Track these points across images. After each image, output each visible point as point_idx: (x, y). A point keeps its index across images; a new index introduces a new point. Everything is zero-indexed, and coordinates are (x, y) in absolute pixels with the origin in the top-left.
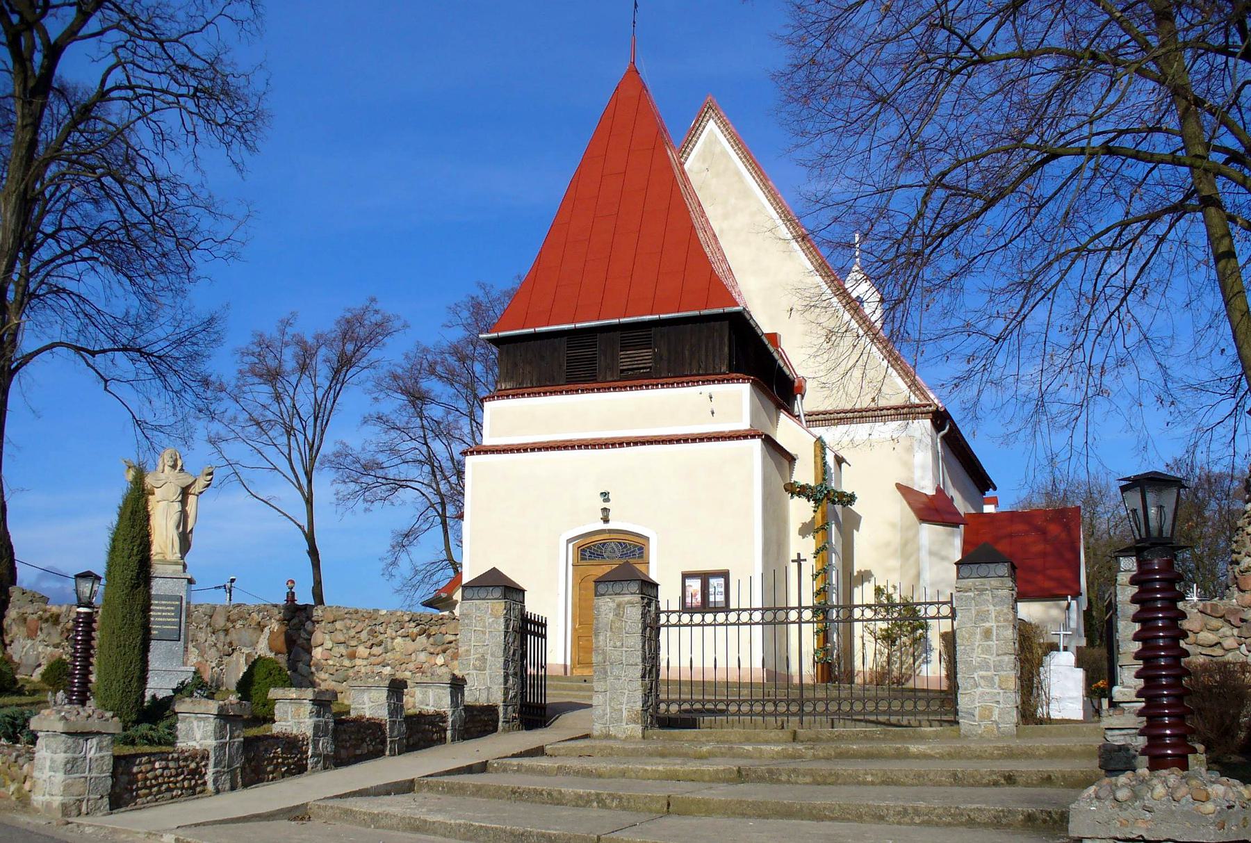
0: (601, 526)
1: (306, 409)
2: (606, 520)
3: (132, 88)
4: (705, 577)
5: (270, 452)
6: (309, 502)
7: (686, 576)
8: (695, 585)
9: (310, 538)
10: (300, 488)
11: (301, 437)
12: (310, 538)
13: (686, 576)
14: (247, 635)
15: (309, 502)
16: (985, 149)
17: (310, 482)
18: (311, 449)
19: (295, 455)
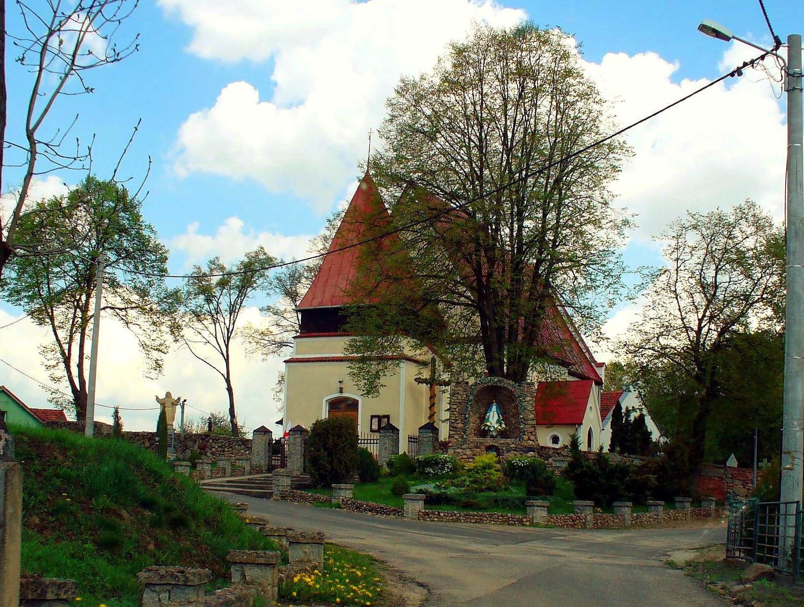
0: (339, 395)
1: (224, 306)
2: (341, 392)
3: (86, 31)
4: (380, 418)
5: (205, 333)
6: (227, 361)
7: (372, 417)
8: (375, 421)
9: (228, 380)
10: (222, 354)
11: (222, 325)
12: (228, 380)
13: (372, 417)
14: (191, 443)
15: (227, 361)
16: (389, 363)
17: (227, 346)
18: (228, 329)
19: (219, 335)
